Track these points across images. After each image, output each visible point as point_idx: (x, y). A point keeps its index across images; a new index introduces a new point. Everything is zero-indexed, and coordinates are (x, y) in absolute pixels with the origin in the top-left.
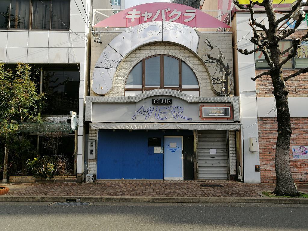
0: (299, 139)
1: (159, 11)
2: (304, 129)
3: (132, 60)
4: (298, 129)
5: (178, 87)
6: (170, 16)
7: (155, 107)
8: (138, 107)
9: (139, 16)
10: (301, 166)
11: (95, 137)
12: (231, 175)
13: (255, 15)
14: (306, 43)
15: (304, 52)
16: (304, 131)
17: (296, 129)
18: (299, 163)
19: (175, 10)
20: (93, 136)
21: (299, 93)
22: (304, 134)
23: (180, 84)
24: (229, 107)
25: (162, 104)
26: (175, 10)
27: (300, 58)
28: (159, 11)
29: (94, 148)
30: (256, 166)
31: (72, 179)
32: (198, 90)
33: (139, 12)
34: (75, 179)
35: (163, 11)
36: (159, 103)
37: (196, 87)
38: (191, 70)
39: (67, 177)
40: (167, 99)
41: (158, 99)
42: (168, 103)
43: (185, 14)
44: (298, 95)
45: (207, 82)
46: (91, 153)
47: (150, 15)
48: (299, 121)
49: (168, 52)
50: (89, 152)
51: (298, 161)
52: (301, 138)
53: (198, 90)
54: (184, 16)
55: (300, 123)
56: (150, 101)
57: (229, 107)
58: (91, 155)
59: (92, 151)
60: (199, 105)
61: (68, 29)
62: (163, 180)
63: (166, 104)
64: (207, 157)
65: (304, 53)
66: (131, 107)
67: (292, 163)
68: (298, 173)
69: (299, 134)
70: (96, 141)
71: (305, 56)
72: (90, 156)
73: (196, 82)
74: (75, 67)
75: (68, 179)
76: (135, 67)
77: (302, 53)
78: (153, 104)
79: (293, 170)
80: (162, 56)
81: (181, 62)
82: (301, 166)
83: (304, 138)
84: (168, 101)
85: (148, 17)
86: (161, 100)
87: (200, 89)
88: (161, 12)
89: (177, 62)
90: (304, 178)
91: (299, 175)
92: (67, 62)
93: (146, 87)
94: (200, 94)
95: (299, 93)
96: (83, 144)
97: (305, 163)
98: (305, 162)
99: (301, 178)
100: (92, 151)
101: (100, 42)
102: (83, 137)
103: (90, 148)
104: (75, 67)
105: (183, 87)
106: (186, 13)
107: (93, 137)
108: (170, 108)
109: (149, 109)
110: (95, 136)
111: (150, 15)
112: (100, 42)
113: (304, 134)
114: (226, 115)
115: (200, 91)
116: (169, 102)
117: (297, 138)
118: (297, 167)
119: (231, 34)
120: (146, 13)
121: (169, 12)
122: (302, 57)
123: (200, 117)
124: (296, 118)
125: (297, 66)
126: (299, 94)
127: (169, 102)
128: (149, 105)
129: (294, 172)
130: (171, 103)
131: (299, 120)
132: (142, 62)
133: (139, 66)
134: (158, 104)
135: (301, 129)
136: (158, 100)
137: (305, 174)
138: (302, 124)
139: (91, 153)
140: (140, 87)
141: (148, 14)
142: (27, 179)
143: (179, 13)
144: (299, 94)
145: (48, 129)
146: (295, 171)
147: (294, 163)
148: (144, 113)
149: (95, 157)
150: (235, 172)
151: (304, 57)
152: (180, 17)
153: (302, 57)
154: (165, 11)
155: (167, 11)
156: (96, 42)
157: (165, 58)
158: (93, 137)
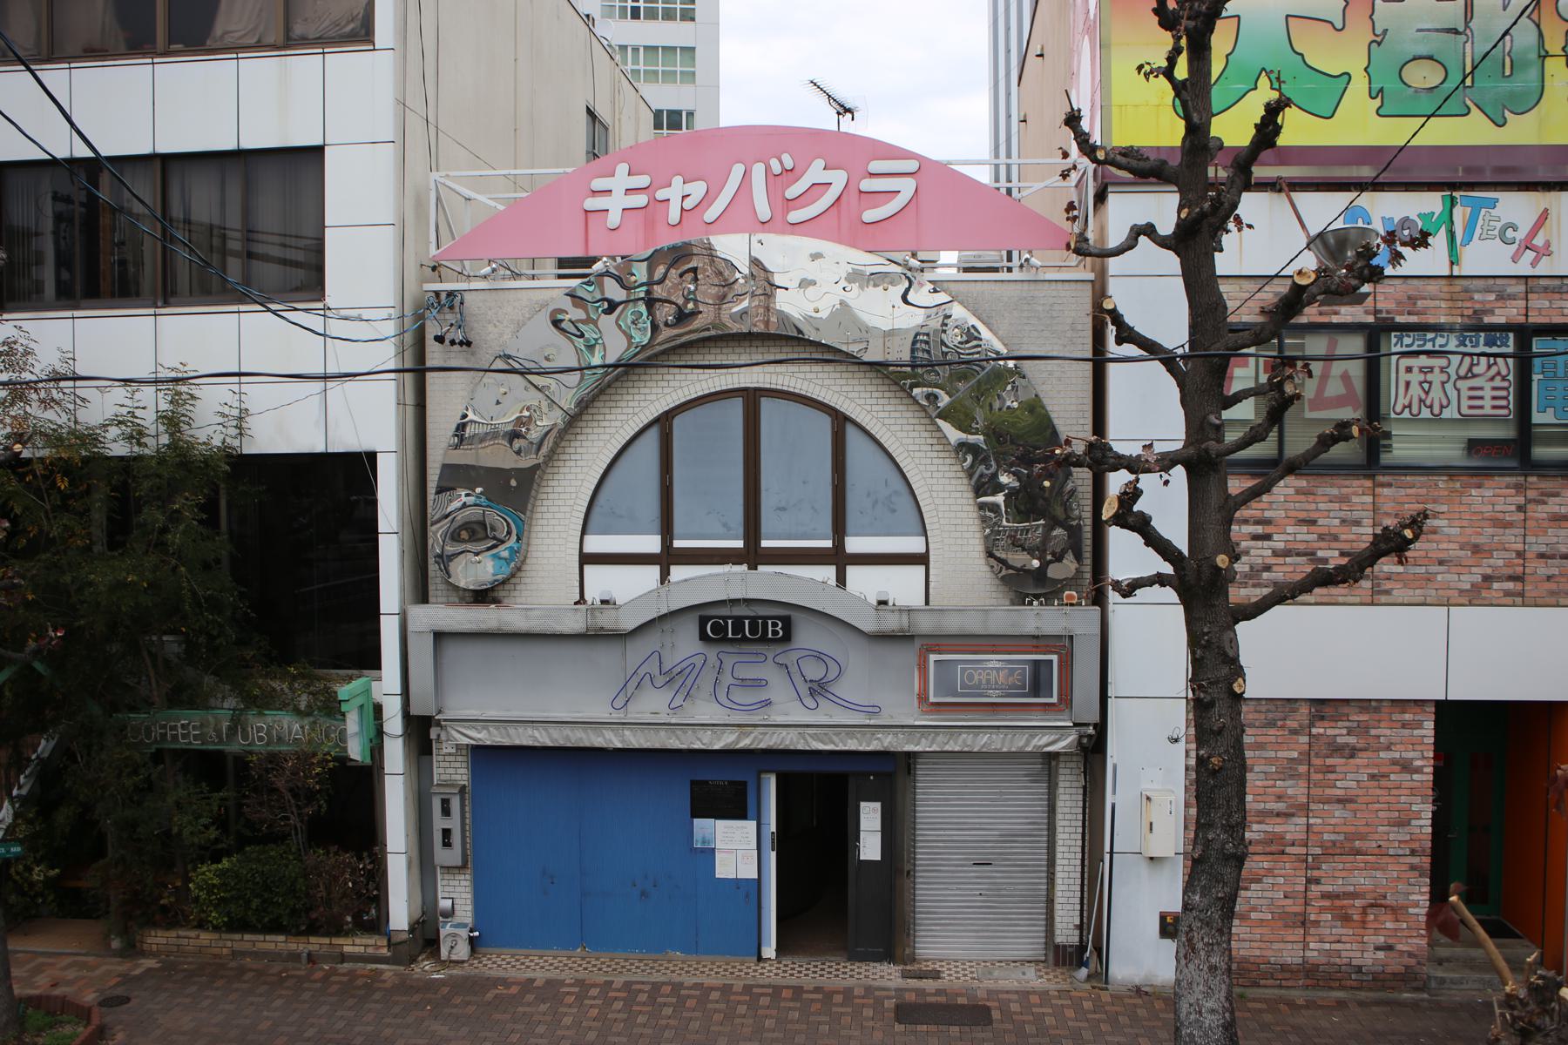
0: (1369, 799)
1: (738, 171)
2: (1397, 755)
3: (613, 417)
4: (1369, 754)
5: (828, 544)
6: (793, 191)
7: (712, 653)
8: (638, 651)
9: (640, 200)
10: (1364, 913)
11: (459, 771)
12: (1057, 947)
13: (853, 572)
14: (1437, 345)
15: (1426, 386)
16: (1394, 762)
17: (1361, 754)
18: (1358, 903)
19: (819, 163)
20: (451, 770)
21: (1387, 585)
22: (1393, 777)
23: (839, 529)
24: (1054, 658)
25: (745, 639)
26: (819, 163)
27: (1406, 414)
28: (738, 171)
29: (454, 823)
30: (1163, 917)
31: (370, 950)
32: (922, 559)
33: (643, 181)
34: (385, 951)
35: (758, 171)
36: (730, 636)
37: (914, 545)
38: (895, 469)
39: (349, 941)
40: (765, 618)
41: (725, 618)
42: (770, 636)
43: (867, 185)
44: (1383, 599)
45: (967, 521)
46: (447, 843)
47: (698, 190)
48: (1377, 717)
49: (781, 377)
50: (438, 838)
51: (1354, 895)
52: (1379, 792)
53: (922, 559)
54: (861, 192)
55: (1383, 724)
56: (690, 629)
57: (1054, 658)
58: (447, 851)
59: (446, 833)
60: (917, 643)
61: (321, 296)
62: (755, 958)
63: (764, 639)
64: (928, 865)
65: (1427, 393)
66: (605, 656)
67: (1327, 903)
68: (1348, 946)
69: (1372, 777)
70: (463, 789)
71: (1431, 407)
72: (442, 856)
73: (920, 529)
74: (360, 467)
75: (357, 949)
76: (631, 450)
77: (1415, 391)
78: (703, 636)
79: (1328, 931)
80: (752, 398)
81: (840, 422)
82: (1364, 913)
83: (1394, 792)
84: (770, 629)
85: (688, 204)
86: (738, 622)
87: (932, 558)
88: (747, 174)
89: (825, 423)
90: (1373, 964)
91: (1352, 954)
92: (319, 448)
93: (677, 544)
94: (931, 578)
95: (1387, 585)
96: (406, 806)
97: (1383, 902)
98: (1385, 897)
99: (1360, 967)
100: (446, 833)
101: (461, 343)
102: (405, 778)
103: (439, 823)
104: (360, 467)
105: (854, 545)
106: (872, 175)
107: (452, 771)
108: (779, 660)
109: (684, 665)
110: (458, 765)
111: (698, 190)
112: (461, 343)
113: (1393, 777)
114: (1036, 695)
115: (931, 566)
116: (775, 633)
117: (1360, 792)
118: (1346, 919)
119: (1089, 286)
120: (677, 181)
121: (790, 174)
122: (1415, 411)
123: (923, 698)
124: (1367, 704)
125: (1395, 452)
126: (1387, 592)
127: (775, 633)
128: (685, 644)
129: (1332, 938)
130: (787, 637)
131: (1377, 710)
132: (664, 422)
133: (652, 439)
134: (724, 640)
135: (1382, 754)
136: (727, 624)
137: (1378, 948)
138: (1388, 732)
139: (447, 843)
140: (651, 544)
141: (689, 188)
142: (197, 943)
143: (838, 179)
144: (1387, 592)
145: (261, 739)
146: (1337, 938)
147: (1338, 903)
148: (660, 681)
149: (464, 856)
150: (1077, 932)
151: (1426, 413)
152: (839, 199)
153: (1415, 411)
154: (768, 169)
155: (776, 168)
156: (447, 342)
157: (766, 404)
158: (452, 771)
